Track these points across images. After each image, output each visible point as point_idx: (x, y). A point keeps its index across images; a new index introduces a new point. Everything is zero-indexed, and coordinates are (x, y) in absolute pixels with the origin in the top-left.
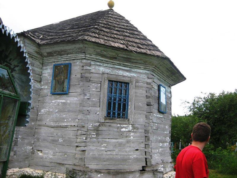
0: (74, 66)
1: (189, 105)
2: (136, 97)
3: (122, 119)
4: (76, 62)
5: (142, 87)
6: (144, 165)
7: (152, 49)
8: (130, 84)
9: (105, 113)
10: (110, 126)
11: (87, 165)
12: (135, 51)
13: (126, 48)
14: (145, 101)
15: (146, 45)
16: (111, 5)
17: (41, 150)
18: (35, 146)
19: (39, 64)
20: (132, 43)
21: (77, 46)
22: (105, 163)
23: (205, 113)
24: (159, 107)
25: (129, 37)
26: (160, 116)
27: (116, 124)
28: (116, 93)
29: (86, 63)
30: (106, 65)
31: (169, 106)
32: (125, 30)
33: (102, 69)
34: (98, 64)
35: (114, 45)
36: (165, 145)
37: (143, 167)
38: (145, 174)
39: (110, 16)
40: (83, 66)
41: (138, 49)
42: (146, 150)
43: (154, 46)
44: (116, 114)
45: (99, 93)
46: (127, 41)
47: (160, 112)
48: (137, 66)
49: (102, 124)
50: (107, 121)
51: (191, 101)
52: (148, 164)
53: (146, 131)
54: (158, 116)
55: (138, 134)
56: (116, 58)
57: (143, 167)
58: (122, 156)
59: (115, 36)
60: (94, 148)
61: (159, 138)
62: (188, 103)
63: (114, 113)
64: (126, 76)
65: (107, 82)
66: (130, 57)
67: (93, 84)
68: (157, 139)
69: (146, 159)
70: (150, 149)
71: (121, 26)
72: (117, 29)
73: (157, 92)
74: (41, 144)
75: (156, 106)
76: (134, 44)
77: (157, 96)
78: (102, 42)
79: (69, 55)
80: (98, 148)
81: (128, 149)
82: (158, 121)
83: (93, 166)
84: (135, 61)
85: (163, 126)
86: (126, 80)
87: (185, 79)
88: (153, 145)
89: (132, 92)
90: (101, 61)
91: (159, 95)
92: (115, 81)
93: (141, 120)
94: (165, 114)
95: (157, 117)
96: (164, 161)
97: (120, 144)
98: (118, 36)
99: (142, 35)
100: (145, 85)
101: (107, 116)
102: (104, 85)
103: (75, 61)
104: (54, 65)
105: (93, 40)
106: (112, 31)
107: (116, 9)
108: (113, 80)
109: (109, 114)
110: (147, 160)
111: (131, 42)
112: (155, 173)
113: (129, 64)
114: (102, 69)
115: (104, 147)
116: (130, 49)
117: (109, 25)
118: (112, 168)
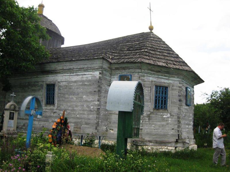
0: (134, 76)
1: (207, 96)
2: (173, 96)
3: (164, 110)
4: (135, 74)
5: (175, 89)
6: (177, 138)
7: (182, 65)
8: (168, 88)
9: (153, 106)
10: (156, 114)
11: (143, 138)
12: (172, 68)
13: (167, 66)
14: (178, 98)
15: (178, 62)
16: (151, 28)
17: (112, 129)
18: (108, 127)
19: (109, 74)
20: (169, 61)
21: (137, 65)
22: (154, 137)
23: (219, 103)
24: (186, 102)
25: (167, 56)
26: (187, 107)
27: (161, 113)
28: (159, 94)
29: (141, 75)
30: (154, 76)
31: (193, 100)
32: (164, 51)
33: (151, 79)
34: (149, 75)
35: (159, 64)
36: (190, 127)
37: (177, 140)
38: (179, 144)
39: (152, 39)
40: (140, 77)
41: (174, 66)
42: (179, 129)
43: (184, 62)
44: (160, 107)
45: (150, 94)
46: (166, 60)
47: (187, 105)
48: (173, 76)
49: (152, 113)
50: (155, 111)
51: (210, 94)
52: (180, 138)
53: (179, 118)
54: (185, 108)
55: (173, 119)
56: (160, 72)
57: (177, 140)
58: (164, 133)
59: (159, 56)
60: (147, 128)
61: (186, 122)
62: (207, 94)
63: (159, 106)
64: (166, 83)
65: (154, 87)
66: (169, 71)
67: (146, 88)
68: (185, 122)
69: (178, 135)
70: (181, 129)
71: (161, 48)
72: (159, 50)
73: (185, 92)
74: (112, 125)
75: (184, 101)
76: (171, 62)
77: (185, 95)
78: (152, 62)
79: (130, 70)
80: (150, 127)
81: (167, 128)
82: (186, 111)
83: (147, 138)
84: (172, 73)
85: (188, 114)
86: (166, 85)
87: (204, 82)
88: (183, 126)
89: (170, 93)
90: (151, 74)
91: (186, 94)
92: (159, 86)
93: (176, 110)
94: (190, 106)
95: (185, 108)
96: (189, 138)
97: (163, 125)
98: (160, 56)
99: (175, 54)
100: (178, 88)
101: (155, 108)
102: (153, 89)
103: (134, 73)
104: (120, 76)
105: (147, 61)
106: (156, 52)
107: (154, 31)
108: (158, 85)
109: (156, 106)
110: (179, 136)
111: (169, 60)
112: (184, 143)
113: (168, 75)
114: (151, 79)
115: (153, 127)
116: (169, 66)
117: (153, 48)
118: (158, 140)
